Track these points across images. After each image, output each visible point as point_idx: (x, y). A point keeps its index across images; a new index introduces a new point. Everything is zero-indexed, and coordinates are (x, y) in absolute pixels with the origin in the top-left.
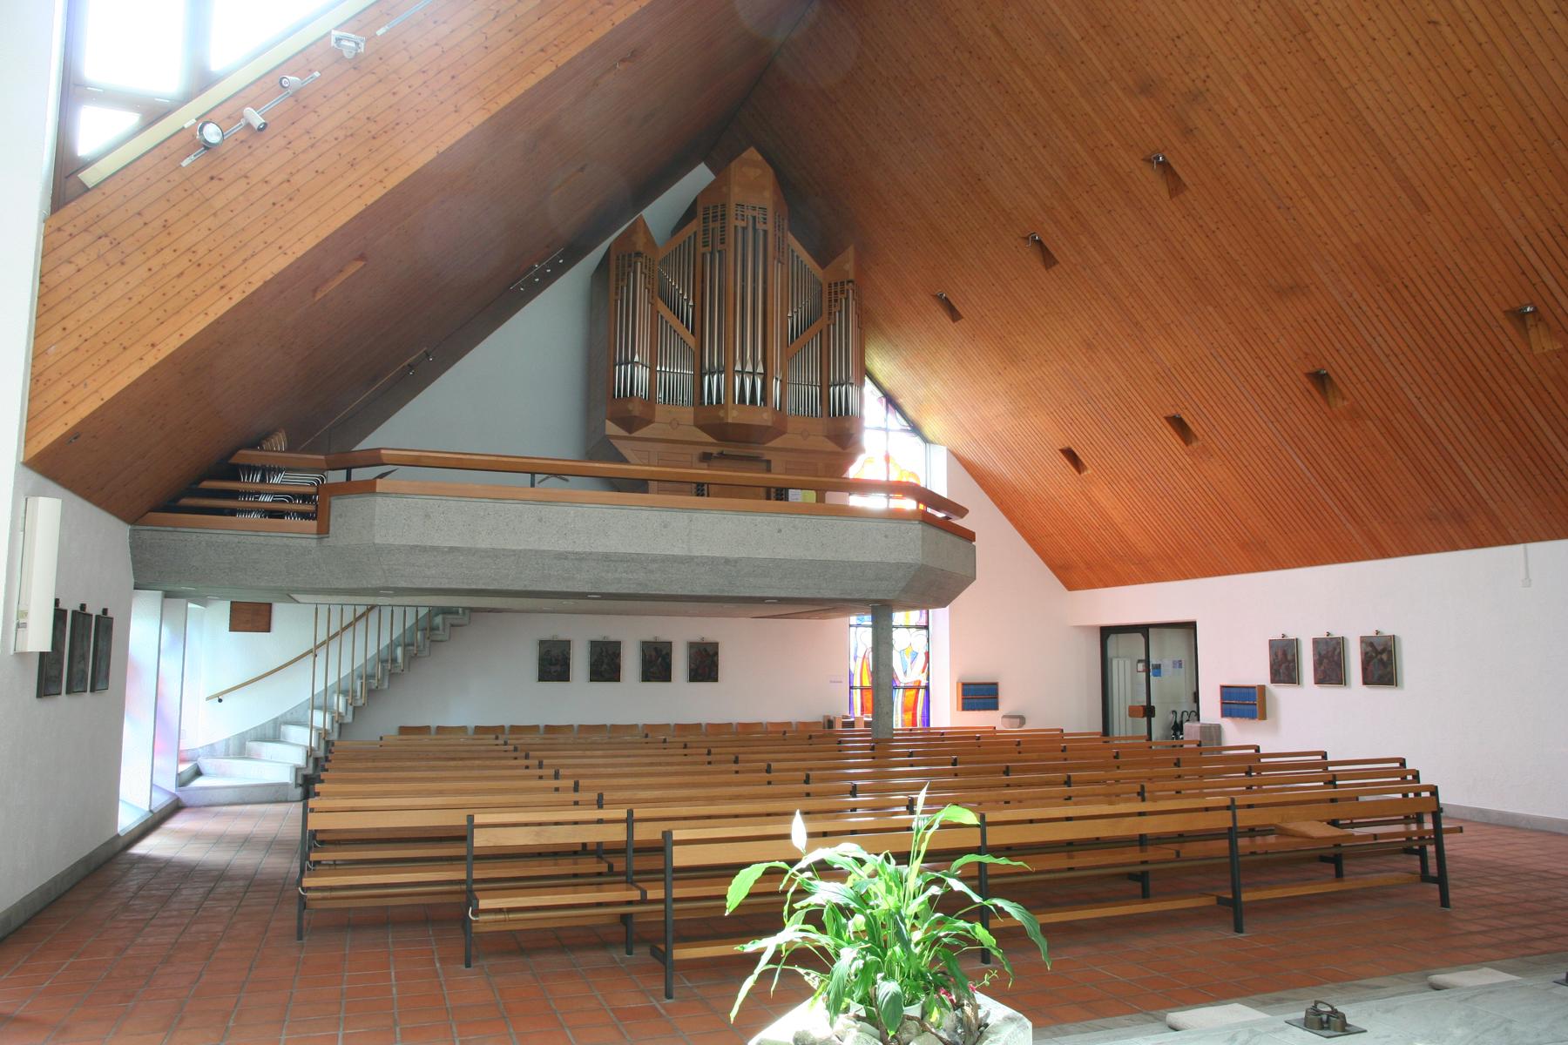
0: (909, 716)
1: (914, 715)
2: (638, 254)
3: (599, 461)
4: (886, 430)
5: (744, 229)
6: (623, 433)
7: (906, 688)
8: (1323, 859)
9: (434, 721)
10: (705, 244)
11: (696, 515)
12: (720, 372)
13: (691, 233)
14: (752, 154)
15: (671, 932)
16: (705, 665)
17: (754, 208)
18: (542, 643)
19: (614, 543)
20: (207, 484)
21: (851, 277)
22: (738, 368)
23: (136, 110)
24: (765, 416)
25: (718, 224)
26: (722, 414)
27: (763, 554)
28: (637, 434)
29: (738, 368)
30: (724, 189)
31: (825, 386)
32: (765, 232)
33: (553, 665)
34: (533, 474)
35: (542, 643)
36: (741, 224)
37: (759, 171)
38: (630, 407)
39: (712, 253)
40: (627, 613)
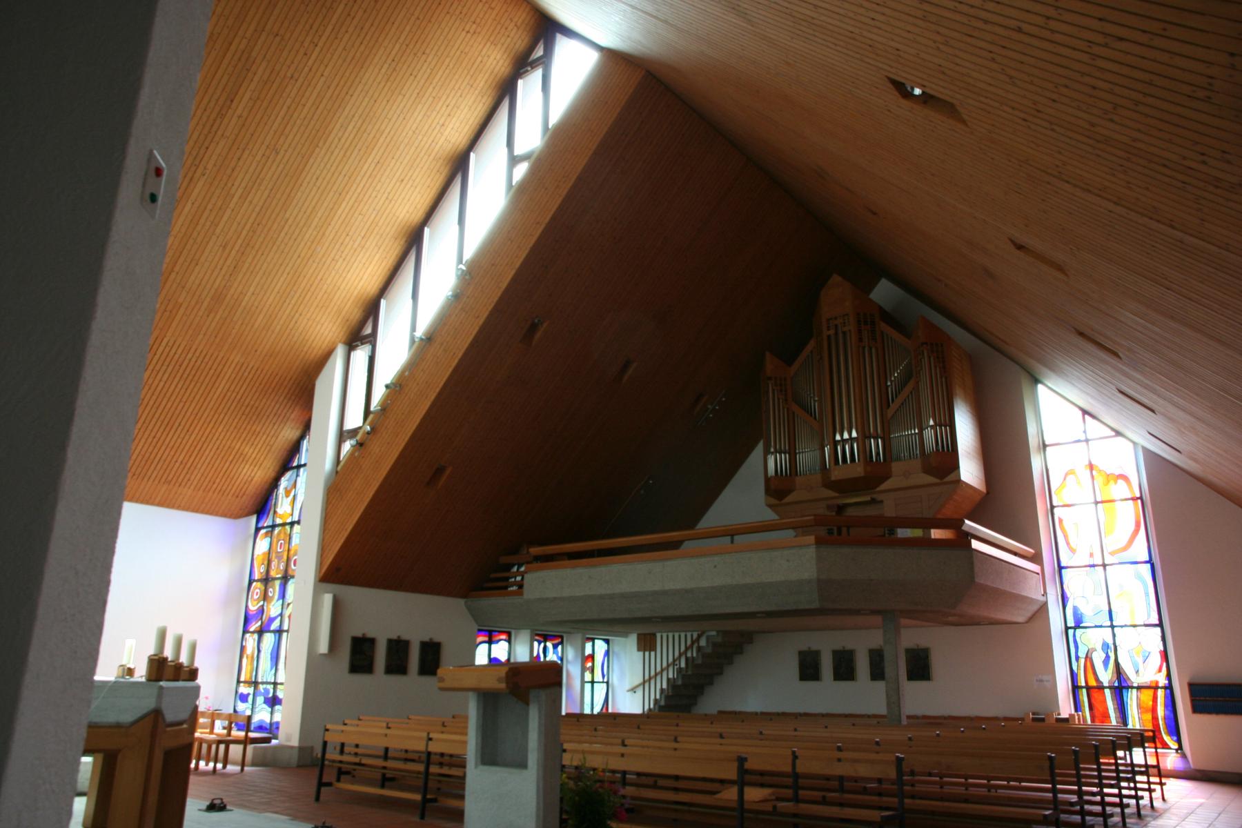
0: (1149, 716)
1: (1155, 718)
3: (570, 542)
4: (1087, 441)
6: (937, 481)
7: (1139, 688)
9: (738, 708)
11: (668, 563)
14: (836, 278)
15: (432, 790)
16: (919, 666)
18: (800, 653)
19: (624, 587)
20: (493, 576)
27: (705, 584)
28: (787, 500)
33: (809, 669)
34: (732, 536)
35: (800, 653)
40: (842, 629)
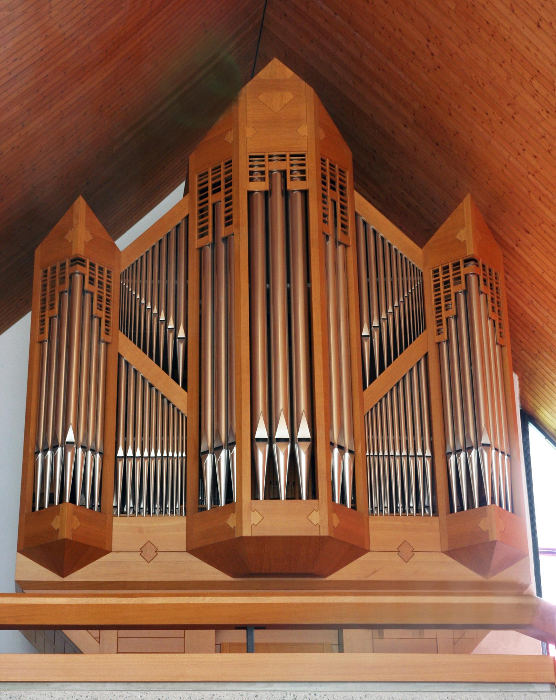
2: (78, 261)
5: (267, 194)
8: (107, 346)
10: (203, 233)
12: (230, 446)
13: (379, 378)
14: (276, 70)
17: (283, 157)
21: (471, 251)
22: (262, 432)
23: (258, 644)
24: (316, 518)
25: (221, 196)
26: (231, 522)
29: (262, 432)
30: (229, 137)
31: (440, 454)
32: (305, 193)
36: (259, 186)
37: (289, 96)
38: (56, 524)
39: (214, 245)
